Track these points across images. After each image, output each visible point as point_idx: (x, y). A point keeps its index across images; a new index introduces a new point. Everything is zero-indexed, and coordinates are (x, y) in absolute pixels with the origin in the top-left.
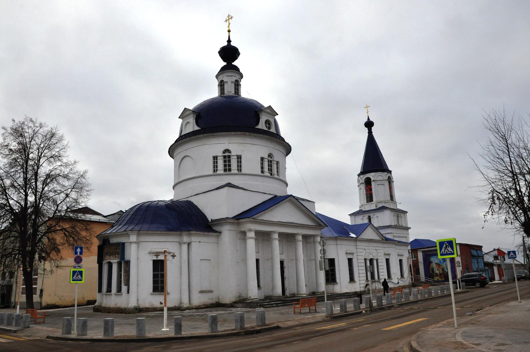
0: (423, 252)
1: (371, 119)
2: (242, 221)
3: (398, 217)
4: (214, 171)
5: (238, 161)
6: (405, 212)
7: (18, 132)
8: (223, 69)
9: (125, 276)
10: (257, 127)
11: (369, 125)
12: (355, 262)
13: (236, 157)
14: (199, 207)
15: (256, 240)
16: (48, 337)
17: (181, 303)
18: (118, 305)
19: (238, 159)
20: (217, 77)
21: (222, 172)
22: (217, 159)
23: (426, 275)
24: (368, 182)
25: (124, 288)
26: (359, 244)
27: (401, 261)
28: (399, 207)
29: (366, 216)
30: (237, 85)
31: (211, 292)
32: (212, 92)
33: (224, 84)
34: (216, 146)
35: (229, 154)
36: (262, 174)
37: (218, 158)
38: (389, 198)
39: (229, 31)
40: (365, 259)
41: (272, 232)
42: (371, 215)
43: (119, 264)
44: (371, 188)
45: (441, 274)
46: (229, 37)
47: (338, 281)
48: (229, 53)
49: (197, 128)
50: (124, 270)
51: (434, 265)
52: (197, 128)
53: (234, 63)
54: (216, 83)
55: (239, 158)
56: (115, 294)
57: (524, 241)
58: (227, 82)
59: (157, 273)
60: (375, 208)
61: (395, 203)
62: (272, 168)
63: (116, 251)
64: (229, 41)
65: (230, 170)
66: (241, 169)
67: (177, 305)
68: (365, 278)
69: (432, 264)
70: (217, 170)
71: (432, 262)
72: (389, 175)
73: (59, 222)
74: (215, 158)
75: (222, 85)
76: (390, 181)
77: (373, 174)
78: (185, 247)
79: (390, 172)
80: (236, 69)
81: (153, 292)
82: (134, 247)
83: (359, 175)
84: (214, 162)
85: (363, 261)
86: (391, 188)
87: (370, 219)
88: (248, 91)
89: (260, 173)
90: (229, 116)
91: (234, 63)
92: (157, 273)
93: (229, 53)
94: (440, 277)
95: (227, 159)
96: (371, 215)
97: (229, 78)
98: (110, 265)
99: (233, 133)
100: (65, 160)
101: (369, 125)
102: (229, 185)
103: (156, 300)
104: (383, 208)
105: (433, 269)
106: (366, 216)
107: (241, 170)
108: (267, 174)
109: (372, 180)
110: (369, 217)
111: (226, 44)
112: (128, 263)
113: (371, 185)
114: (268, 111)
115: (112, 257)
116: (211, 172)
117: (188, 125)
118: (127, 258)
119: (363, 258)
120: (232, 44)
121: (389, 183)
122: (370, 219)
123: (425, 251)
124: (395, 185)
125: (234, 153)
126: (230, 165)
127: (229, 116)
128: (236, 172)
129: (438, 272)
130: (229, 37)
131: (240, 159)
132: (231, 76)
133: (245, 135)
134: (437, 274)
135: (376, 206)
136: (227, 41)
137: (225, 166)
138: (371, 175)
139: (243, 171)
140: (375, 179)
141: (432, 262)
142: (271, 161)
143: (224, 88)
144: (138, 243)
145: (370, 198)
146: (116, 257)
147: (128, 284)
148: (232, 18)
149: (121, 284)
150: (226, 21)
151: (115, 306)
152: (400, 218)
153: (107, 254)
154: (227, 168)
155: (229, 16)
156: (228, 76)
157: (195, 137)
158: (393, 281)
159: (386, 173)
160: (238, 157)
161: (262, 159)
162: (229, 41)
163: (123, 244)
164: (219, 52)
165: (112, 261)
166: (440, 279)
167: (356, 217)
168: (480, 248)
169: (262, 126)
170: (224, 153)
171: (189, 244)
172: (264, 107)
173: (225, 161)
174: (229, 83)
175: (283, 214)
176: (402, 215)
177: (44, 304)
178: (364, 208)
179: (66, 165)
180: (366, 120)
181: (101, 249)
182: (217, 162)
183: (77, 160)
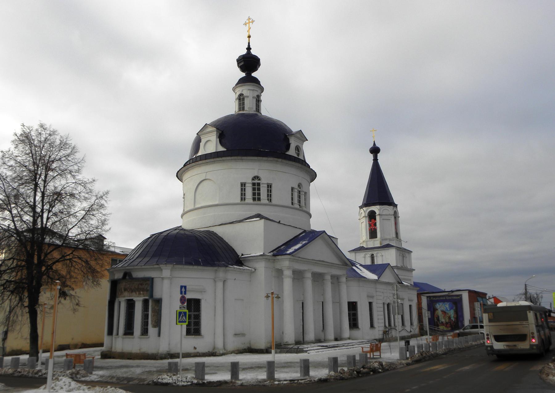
0: (427, 297)
1: (377, 145)
2: (279, 257)
3: (403, 257)
4: (242, 199)
5: (268, 190)
6: (410, 252)
7: (25, 139)
8: (242, 81)
9: (153, 316)
10: (287, 153)
11: (375, 151)
12: (374, 306)
13: (266, 186)
14: (225, 239)
15: (294, 279)
16: (216, 373)
17: (214, 348)
18: (143, 351)
19: (268, 187)
20: (234, 89)
21: (251, 201)
22: (245, 186)
23: (429, 324)
24: (372, 216)
25: (152, 331)
26: (378, 286)
27: (410, 306)
28: (404, 246)
29: (369, 254)
30: (258, 100)
31: (243, 335)
32: (230, 108)
33: (243, 99)
34: (244, 170)
35: (259, 182)
36: (292, 206)
37: (247, 185)
38: (394, 236)
39: (249, 37)
40: (384, 304)
41: (305, 271)
42: (375, 253)
43: (146, 302)
44: (376, 223)
45: (447, 323)
46: (249, 43)
47: (360, 326)
48: (249, 63)
49: (221, 149)
50: (152, 309)
51: (439, 313)
52: (221, 149)
53: (254, 74)
54: (233, 97)
55: (269, 186)
56: (139, 338)
57: (526, 290)
58: (248, 97)
59: (195, 313)
60: (379, 246)
61: (400, 241)
62: (300, 199)
63: (140, 287)
64: (249, 49)
65: (259, 199)
66: (271, 200)
67: (211, 350)
68: (383, 325)
69: (437, 311)
70: (245, 199)
71: (437, 310)
72: (395, 209)
73: (74, 251)
74: (243, 185)
75: (241, 99)
76: (396, 215)
77: (378, 207)
78: (220, 285)
79: (396, 206)
80: (256, 81)
81: (187, 335)
82: (166, 283)
83: (361, 207)
84: (242, 189)
85: (382, 305)
86: (396, 224)
87: (372, 257)
88: (271, 109)
89: (290, 205)
90: (253, 138)
91: (254, 74)
92: (195, 313)
93: (249, 63)
94: (446, 327)
95: (256, 187)
96: (375, 253)
97: (246, 90)
98: (131, 305)
99: (264, 158)
100: (79, 177)
101: (375, 151)
102: (259, 216)
103: (191, 344)
104: (388, 246)
105: (438, 316)
106: (369, 254)
107: (271, 201)
108: (297, 206)
109: (377, 213)
110: (372, 255)
111: (244, 52)
112: (158, 302)
113: (375, 219)
114: (298, 135)
115: (134, 293)
116: (238, 200)
117: (208, 144)
118: (157, 295)
119: (381, 302)
120: (253, 52)
121: (395, 218)
122: (372, 257)
123: (430, 297)
124: (401, 220)
125: (264, 181)
126: (259, 194)
127: (253, 138)
128: (267, 202)
129: (443, 320)
130: (249, 43)
131: (271, 188)
132: (253, 90)
133: (277, 161)
134: (442, 322)
135: (381, 244)
136: (247, 49)
137: (254, 194)
138: (376, 209)
139: (274, 201)
140: (381, 213)
141: (437, 310)
142: (300, 191)
143: (243, 104)
144: (171, 278)
145: (373, 234)
146: (140, 294)
147: (158, 324)
148: (253, 22)
149: (147, 325)
150: (245, 24)
151: (138, 352)
152: (405, 258)
153: (125, 290)
154: (256, 197)
155: (249, 19)
156: (249, 90)
157: (220, 159)
158: (406, 328)
159: (392, 207)
160: (268, 186)
161: (292, 189)
162: (249, 49)
163: (153, 279)
164: (238, 60)
165: (135, 299)
166: (445, 329)
167: (357, 254)
168: (486, 294)
169: (292, 152)
170: (253, 179)
171: (224, 282)
172: (292, 132)
173: (254, 189)
174: (251, 98)
175: (316, 251)
176: (407, 255)
177: (8, 349)
178: (367, 245)
179: (84, 184)
180: (372, 145)
181: (114, 284)
182: (245, 189)
183: (96, 179)
